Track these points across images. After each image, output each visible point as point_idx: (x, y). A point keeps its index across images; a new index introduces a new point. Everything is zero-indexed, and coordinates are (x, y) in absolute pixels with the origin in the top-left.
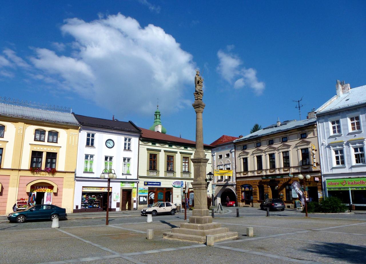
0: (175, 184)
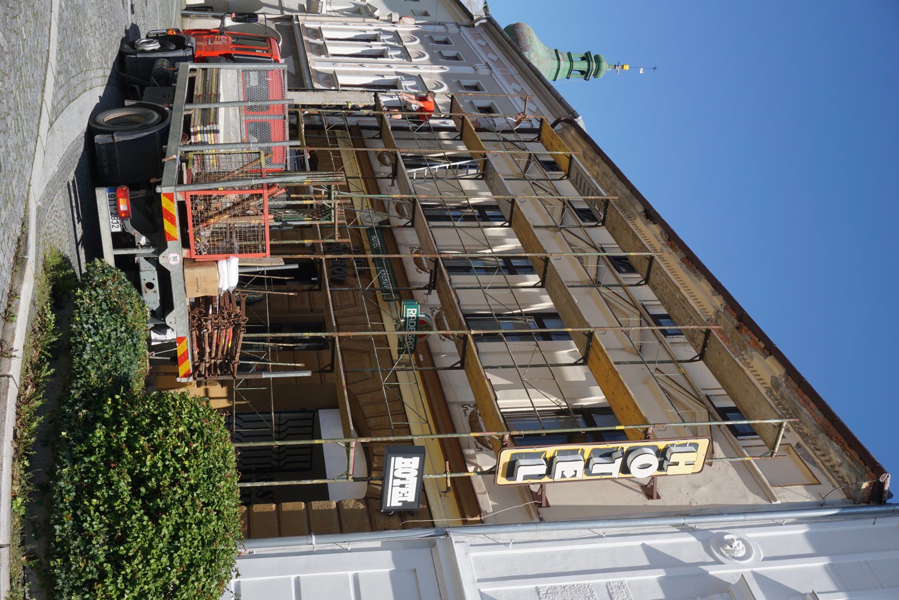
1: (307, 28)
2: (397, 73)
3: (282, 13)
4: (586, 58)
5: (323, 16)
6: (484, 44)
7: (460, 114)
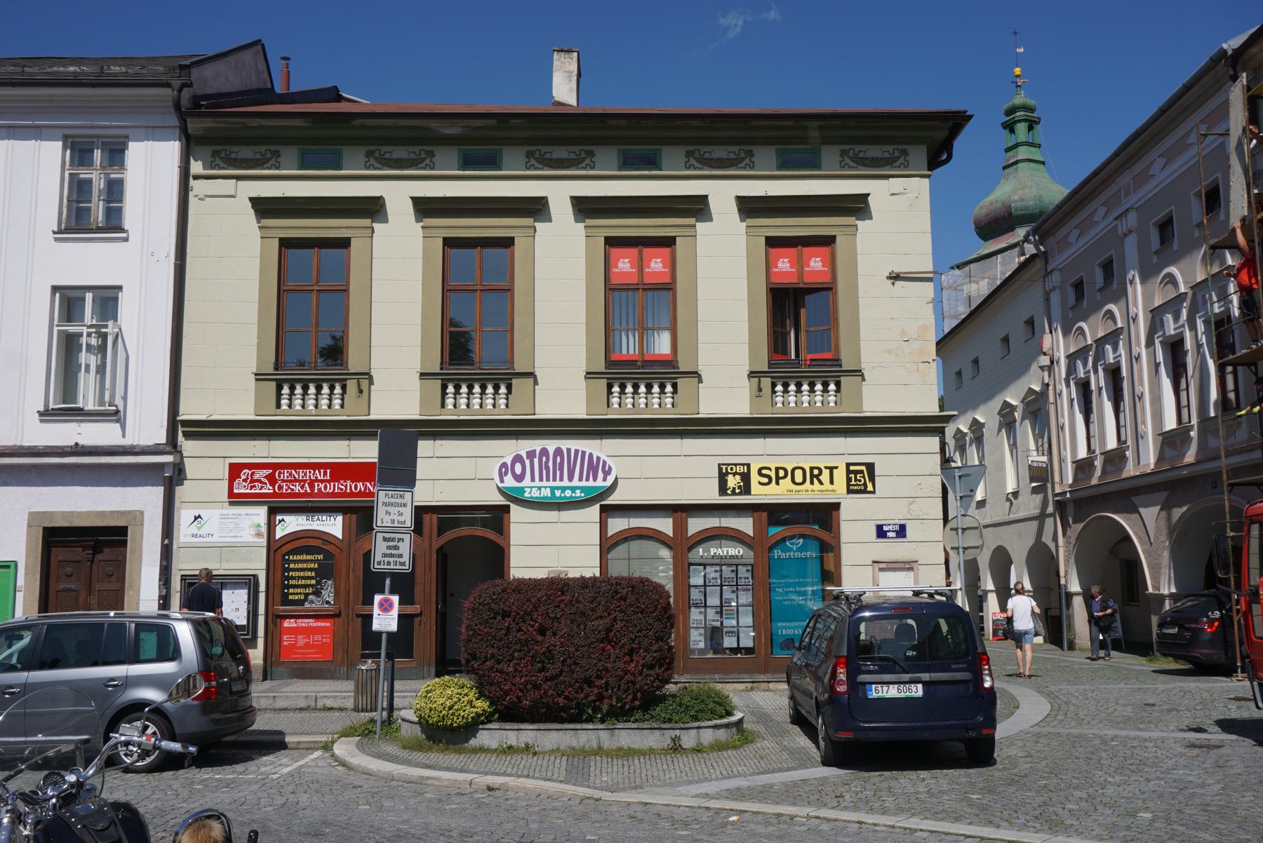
0: (519, 478)
1: (1075, 479)
2: (1150, 343)
3: (1050, 515)
4: (1010, 127)
5: (1051, 459)
6: (1076, 232)
7: (1255, 226)
